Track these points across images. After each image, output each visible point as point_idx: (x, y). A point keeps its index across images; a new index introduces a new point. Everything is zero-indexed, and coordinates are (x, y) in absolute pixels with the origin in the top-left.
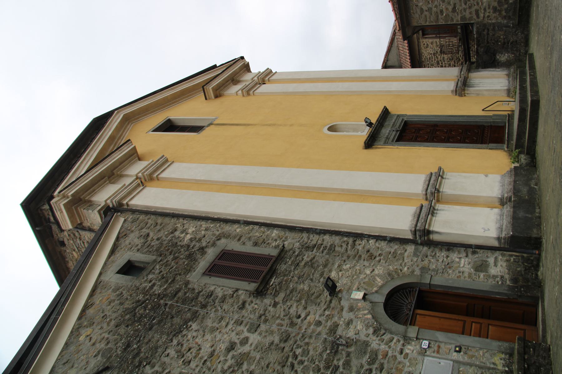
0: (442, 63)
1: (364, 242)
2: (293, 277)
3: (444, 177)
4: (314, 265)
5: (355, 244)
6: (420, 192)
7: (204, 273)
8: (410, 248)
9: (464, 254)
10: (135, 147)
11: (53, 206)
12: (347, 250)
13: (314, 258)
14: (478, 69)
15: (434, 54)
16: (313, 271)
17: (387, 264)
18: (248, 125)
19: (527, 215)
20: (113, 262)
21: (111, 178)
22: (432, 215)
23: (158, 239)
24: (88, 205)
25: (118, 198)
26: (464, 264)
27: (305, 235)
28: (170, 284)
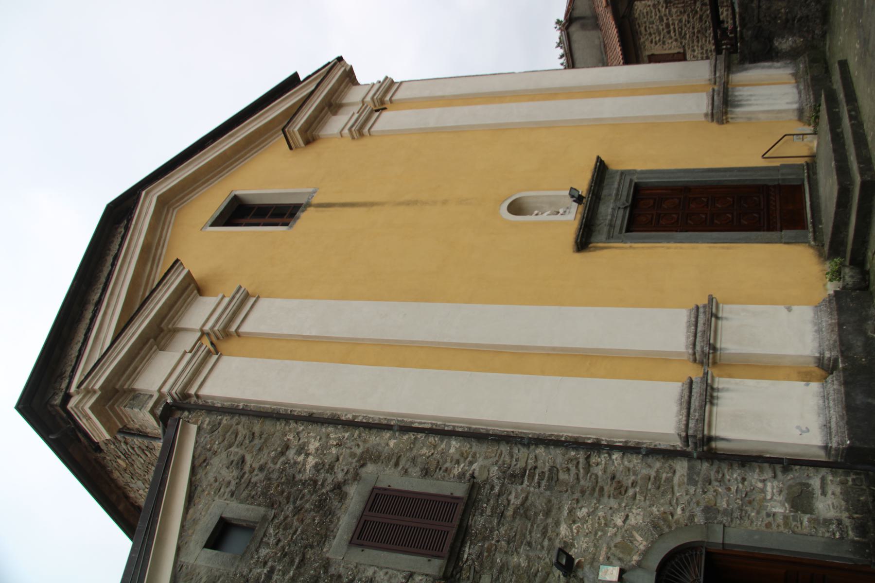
0: (668, 19)
1: (604, 458)
2: (498, 541)
3: (720, 315)
4: (528, 514)
5: (589, 465)
6: (682, 349)
7: (350, 542)
8: (681, 467)
9: (771, 474)
10: (189, 272)
11: (73, 412)
12: (578, 479)
13: (527, 498)
14: (743, 64)
15: (654, 5)
16: (529, 525)
17: (648, 503)
18: (372, 204)
19: (870, 400)
20: (195, 522)
21: (159, 338)
22: (712, 404)
23: (261, 469)
24: (131, 397)
25: (178, 388)
26: (773, 494)
27: (504, 448)
28: (298, 567)
